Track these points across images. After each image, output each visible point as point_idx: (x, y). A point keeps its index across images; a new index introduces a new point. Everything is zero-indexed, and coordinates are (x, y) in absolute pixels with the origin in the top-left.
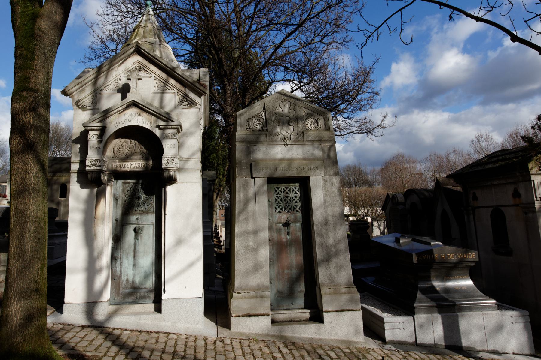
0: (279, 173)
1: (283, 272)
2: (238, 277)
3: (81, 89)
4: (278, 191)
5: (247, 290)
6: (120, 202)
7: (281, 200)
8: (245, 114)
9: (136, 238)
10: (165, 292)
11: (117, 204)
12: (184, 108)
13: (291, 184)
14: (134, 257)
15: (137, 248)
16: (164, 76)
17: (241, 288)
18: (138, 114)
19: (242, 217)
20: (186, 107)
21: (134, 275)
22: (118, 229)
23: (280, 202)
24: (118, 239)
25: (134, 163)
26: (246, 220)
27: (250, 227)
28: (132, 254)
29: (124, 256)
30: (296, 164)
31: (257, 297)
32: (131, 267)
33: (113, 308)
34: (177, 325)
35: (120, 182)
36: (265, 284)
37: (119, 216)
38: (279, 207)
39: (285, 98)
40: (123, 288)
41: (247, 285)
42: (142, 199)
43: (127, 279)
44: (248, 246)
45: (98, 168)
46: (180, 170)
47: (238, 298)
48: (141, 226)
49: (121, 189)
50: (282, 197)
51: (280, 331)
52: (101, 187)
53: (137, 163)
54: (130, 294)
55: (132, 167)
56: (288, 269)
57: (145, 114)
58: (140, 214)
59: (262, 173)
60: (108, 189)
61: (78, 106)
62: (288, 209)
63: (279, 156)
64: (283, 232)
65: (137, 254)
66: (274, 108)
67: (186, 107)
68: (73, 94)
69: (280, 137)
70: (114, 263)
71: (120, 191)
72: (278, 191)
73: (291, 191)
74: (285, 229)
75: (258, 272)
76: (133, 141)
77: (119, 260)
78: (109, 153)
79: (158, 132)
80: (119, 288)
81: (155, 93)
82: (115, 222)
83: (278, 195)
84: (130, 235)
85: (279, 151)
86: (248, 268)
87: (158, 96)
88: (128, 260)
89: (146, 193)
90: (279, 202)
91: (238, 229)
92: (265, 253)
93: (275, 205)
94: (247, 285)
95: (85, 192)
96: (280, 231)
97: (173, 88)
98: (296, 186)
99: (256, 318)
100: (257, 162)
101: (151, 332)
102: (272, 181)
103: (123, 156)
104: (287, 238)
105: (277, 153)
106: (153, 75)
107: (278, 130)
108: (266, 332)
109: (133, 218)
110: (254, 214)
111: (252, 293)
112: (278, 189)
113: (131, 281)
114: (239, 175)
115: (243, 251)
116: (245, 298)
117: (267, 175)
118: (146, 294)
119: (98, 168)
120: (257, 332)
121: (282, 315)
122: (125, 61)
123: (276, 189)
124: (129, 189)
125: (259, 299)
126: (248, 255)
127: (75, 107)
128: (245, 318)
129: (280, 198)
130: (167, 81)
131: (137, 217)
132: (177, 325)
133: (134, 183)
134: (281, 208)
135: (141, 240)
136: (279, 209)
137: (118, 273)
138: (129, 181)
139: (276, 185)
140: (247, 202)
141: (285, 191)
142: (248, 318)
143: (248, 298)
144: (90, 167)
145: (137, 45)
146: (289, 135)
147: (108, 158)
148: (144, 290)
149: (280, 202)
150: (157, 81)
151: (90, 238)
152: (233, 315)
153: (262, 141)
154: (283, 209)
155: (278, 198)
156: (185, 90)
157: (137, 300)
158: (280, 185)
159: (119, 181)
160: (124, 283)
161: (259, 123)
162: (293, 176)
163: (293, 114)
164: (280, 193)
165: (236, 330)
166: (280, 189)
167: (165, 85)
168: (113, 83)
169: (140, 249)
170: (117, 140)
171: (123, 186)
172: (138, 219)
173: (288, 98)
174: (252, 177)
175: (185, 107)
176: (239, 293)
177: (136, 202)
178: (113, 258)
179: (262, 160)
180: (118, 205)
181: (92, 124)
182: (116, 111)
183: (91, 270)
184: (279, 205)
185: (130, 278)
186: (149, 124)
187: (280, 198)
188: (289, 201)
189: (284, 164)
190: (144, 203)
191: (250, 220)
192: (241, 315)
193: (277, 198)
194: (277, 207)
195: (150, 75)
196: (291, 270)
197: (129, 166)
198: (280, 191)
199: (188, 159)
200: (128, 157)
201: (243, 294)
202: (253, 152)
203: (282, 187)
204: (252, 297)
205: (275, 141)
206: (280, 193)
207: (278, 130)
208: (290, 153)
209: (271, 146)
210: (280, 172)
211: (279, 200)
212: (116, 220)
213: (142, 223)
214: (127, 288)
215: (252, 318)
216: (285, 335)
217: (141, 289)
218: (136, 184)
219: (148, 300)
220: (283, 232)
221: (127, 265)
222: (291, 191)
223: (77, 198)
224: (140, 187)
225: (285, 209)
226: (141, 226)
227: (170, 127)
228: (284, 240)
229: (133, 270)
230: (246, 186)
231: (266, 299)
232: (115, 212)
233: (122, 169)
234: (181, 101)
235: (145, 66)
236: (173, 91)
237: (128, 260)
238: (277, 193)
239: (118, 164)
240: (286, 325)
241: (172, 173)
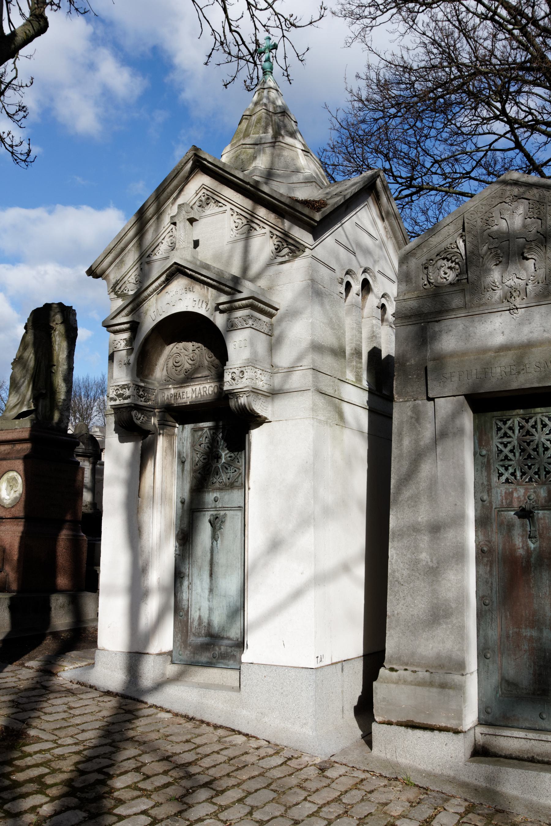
0: (492, 384)
1: (518, 634)
2: (392, 632)
3: (117, 261)
4: (505, 428)
5: (412, 664)
6: (188, 466)
7: (512, 451)
8: (419, 253)
9: (214, 537)
10: (247, 648)
11: (183, 470)
12: (282, 263)
13: (538, 410)
14: (211, 575)
16: (247, 203)
17: (399, 660)
18: (188, 289)
19: (407, 493)
20: (287, 258)
21: (211, 610)
22: (186, 520)
23: (511, 456)
24: (186, 538)
25: (198, 387)
26: (415, 499)
27: (423, 515)
28: (207, 568)
29: (195, 571)
30: (537, 356)
31: (431, 684)
32: (207, 592)
33: (171, 670)
34: (266, 719)
35: (188, 427)
36: (454, 656)
37: (186, 495)
38: (507, 469)
39: (516, 191)
40: (194, 635)
41: (413, 654)
42: (223, 460)
43: (200, 617)
44: (417, 562)
45: (126, 401)
46: (273, 394)
47: (388, 681)
48: (222, 513)
49: (189, 440)
50: (516, 443)
51: (490, 779)
52: (148, 439)
53: (201, 387)
54: (205, 647)
55: (194, 396)
56: (533, 627)
57: (198, 287)
58: (220, 489)
59: (451, 387)
60: (161, 443)
61: (116, 293)
62: (531, 472)
63: (499, 340)
64: (517, 533)
65: (215, 569)
66: (487, 222)
67: (287, 258)
68: (107, 272)
69: (499, 293)
70: (178, 582)
71: (189, 445)
72: (505, 428)
73: (539, 426)
74: (523, 526)
75: (440, 624)
76: (197, 345)
77: (186, 579)
78: (160, 372)
79: (219, 320)
80: (187, 632)
81: (235, 241)
82: (180, 505)
83: (505, 440)
84: (205, 531)
85: (497, 329)
86: (415, 612)
87: (240, 246)
88: (201, 580)
89: (231, 450)
90: (506, 457)
91: (395, 521)
92: (467, 580)
93: (496, 465)
94: (413, 654)
95: (127, 448)
96: (510, 527)
97: (262, 224)
99: (427, 734)
100: (440, 360)
101: (202, 722)
102: (487, 403)
103: (182, 376)
104: (528, 549)
105: (491, 334)
106: (229, 206)
107: (496, 275)
108: (452, 774)
109: (210, 497)
110: (433, 483)
111: (422, 674)
112: (505, 423)
113: (205, 620)
114: (400, 395)
115: (406, 573)
116: (405, 682)
117: (464, 390)
118: (229, 650)
119: (126, 401)
120: (429, 768)
121: (513, 740)
122: (181, 190)
123: (500, 424)
124: (203, 440)
125: (434, 690)
126: (417, 583)
127: (113, 295)
128: (403, 728)
129: (510, 447)
130: (252, 214)
131: (215, 495)
132: (266, 719)
133: (210, 428)
134: (511, 470)
135: (222, 541)
136: (506, 475)
137: (185, 603)
138: (202, 425)
139: (498, 413)
140: (417, 458)
141: (521, 427)
142: (410, 731)
143: (411, 683)
144: (115, 400)
145: (195, 155)
146: (522, 283)
147: (159, 383)
148: (226, 642)
149: (511, 456)
150: (235, 217)
151: (134, 532)
152: (377, 718)
153: (453, 310)
154: (518, 474)
155: (505, 446)
156: (283, 224)
157: (214, 660)
158: (508, 413)
159: (186, 426)
160: (196, 623)
161: (450, 268)
162: (528, 386)
163: (535, 226)
164: (510, 433)
165: (383, 755)
166: (509, 423)
167: (250, 223)
168: (166, 239)
169: (221, 559)
170: (171, 346)
171: (193, 435)
172: (216, 500)
173: (522, 190)
174: (429, 399)
175: (283, 259)
176: (392, 670)
177: (214, 466)
178: (179, 575)
179: (452, 355)
180: (185, 473)
181: (116, 321)
182: (151, 289)
183: (137, 593)
184: (507, 463)
185: (205, 615)
186: (204, 305)
187: (510, 447)
188: (533, 454)
189: (507, 360)
190: (226, 467)
191: (424, 499)
192: (394, 720)
193: (501, 447)
194: (502, 470)
195: (224, 208)
197: (189, 395)
198: (511, 428)
199: (290, 370)
200: (188, 378)
201: (401, 672)
202: (435, 337)
203: (516, 418)
204: (422, 684)
205: (485, 304)
206: (510, 433)
207: (496, 275)
208: (526, 330)
209: (476, 318)
210: (494, 380)
211: (506, 451)
212: (183, 503)
213: (224, 508)
214: (198, 635)
215: (419, 733)
216: (498, 789)
217: (223, 638)
218: (214, 429)
219: (231, 662)
220: (517, 533)
221: (199, 590)
222: (539, 426)
223: (117, 459)
224: (221, 435)
225: (523, 474)
226: (222, 513)
227: (240, 303)
228: (521, 552)
229: (209, 601)
230: (417, 417)
231: (451, 692)
232: (181, 488)
233: (180, 401)
234: (278, 250)
235: (214, 192)
236: (263, 231)
237: (201, 580)
238: (501, 433)
239: (172, 391)
240: (514, 766)
241: (243, 400)
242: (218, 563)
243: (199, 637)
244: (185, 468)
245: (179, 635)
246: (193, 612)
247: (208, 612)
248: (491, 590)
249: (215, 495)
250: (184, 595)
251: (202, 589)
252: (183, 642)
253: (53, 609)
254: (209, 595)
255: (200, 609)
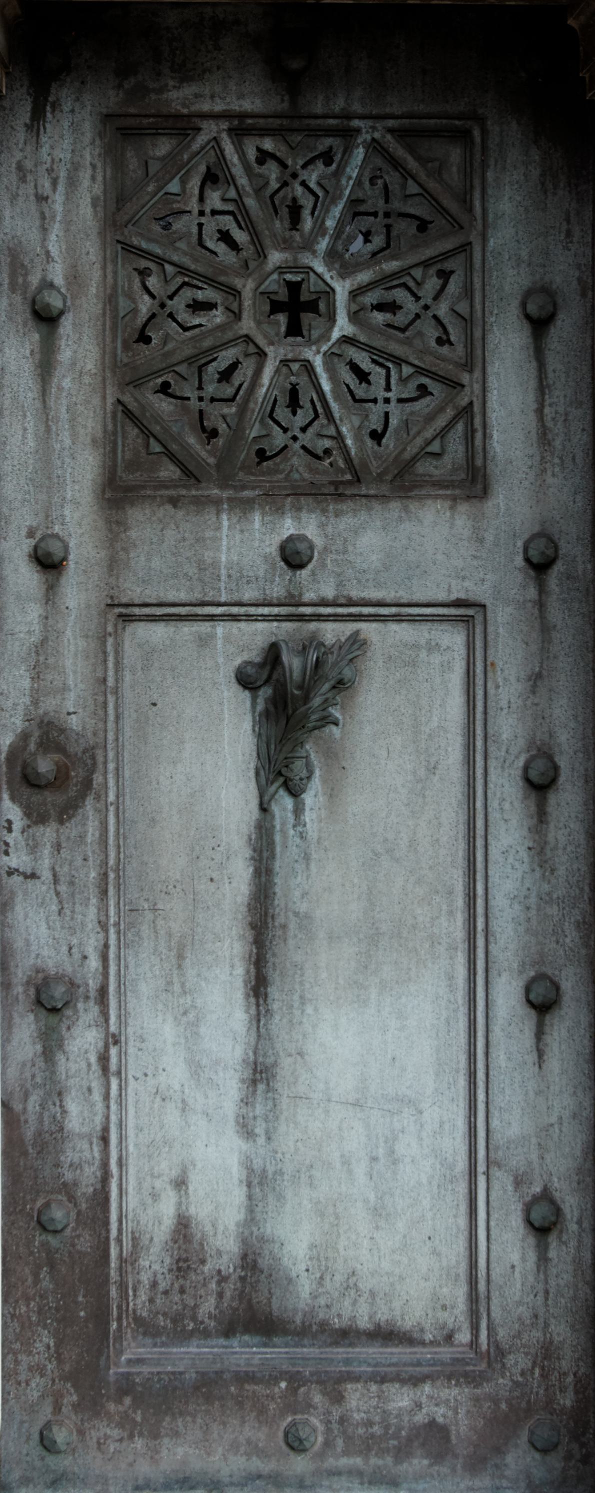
9: (280, 767)
14: (259, 987)
15: (293, 888)
21: (259, 1183)
32: (231, 1087)
43: (183, 1227)
77: (88, 1012)
80: (101, 1316)
98: (293, 145)
113: (223, 1239)
131: (288, 527)
135: (332, 794)
160: (154, 1262)
169: (324, 887)
180: (64, 380)
185: (221, 1214)
196: (396, 1417)
213: (349, 608)
229: (246, 1130)
242: (305, 920)
243: (182, 1336)
244: (65, 354)
245: (46, 1338)
246: (132, 1201)
247: (239, 1195)
248: (119, 917)
249: (288, 527)
250: (73, 1107)
251: (196, 1068)
252: (73, 1378)
253: (307, 808)
254: (246, 1102)
255: (180, 1183)
